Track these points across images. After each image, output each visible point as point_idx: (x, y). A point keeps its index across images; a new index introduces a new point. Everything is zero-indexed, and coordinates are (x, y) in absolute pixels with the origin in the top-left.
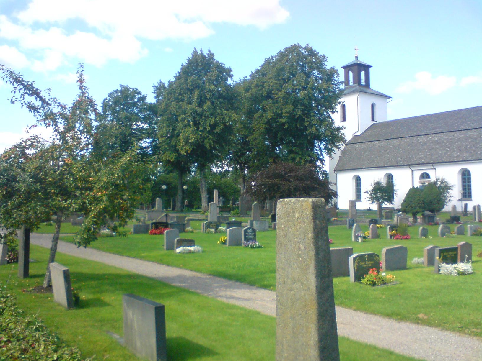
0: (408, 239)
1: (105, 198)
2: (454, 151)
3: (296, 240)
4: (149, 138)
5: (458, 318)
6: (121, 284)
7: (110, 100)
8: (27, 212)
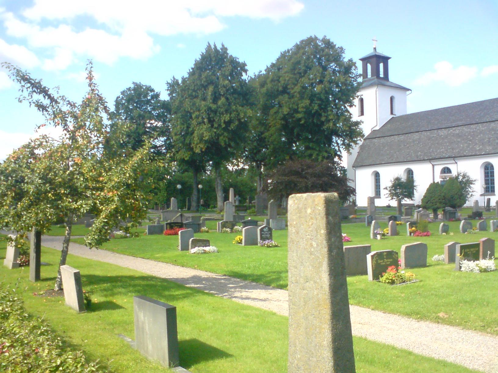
0: (428, 236)
1: (116, 199)
2: (476, 144)
3: (308, 237)
4: (163, 137)
5: (480, 317)
6: (135, 286)
7: (122, 98)
8: (37, 214)
